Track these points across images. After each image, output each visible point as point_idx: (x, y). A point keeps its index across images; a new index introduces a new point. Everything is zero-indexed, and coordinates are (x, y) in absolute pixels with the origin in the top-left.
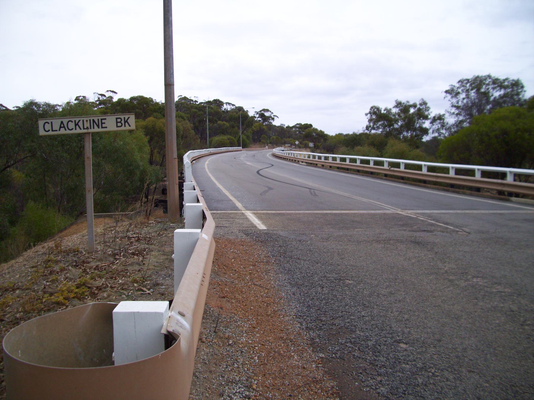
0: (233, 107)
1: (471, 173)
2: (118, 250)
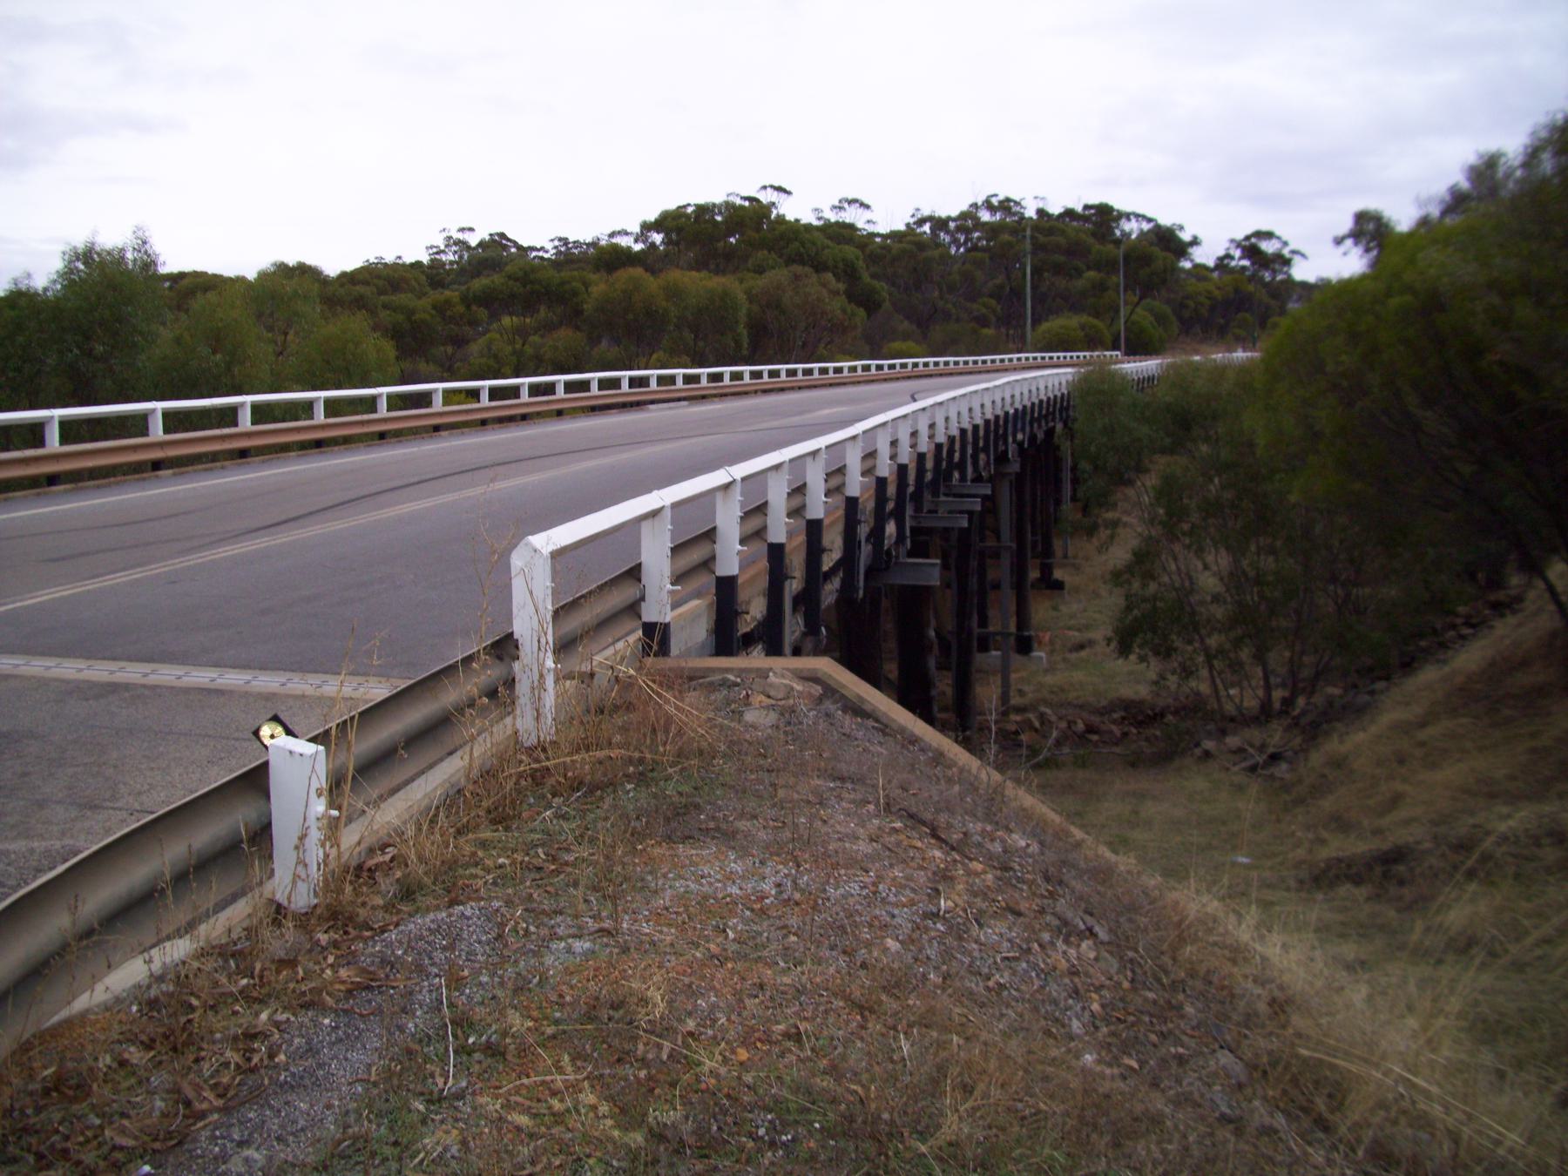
0: (1146, 226)
1: (514, 392)
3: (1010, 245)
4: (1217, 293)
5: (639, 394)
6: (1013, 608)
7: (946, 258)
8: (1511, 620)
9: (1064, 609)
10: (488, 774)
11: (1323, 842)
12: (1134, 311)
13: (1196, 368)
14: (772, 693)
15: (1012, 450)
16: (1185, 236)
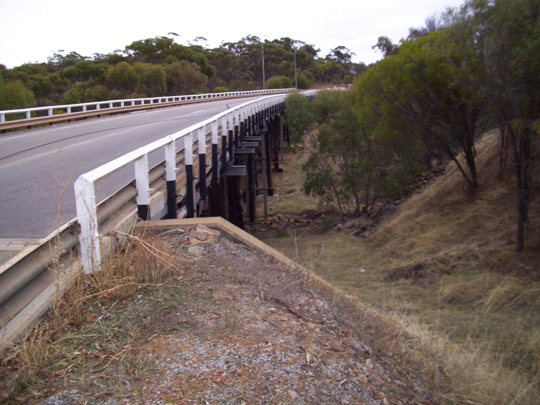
0: (302, 45)
1: (80, 109)
2: (263, 217)
3: (256, 52)
4: (327, 67)
5: (128, 108)
6: (266, 179)
7: (234, 57)
8: (441, 177)
9: (283, 178)
10: (66, 296)
11: (390, 262)
12: (299, 74)
13: (329, 92)
14: (199, 237)
15: (265, 123)
16: (316, 48)
